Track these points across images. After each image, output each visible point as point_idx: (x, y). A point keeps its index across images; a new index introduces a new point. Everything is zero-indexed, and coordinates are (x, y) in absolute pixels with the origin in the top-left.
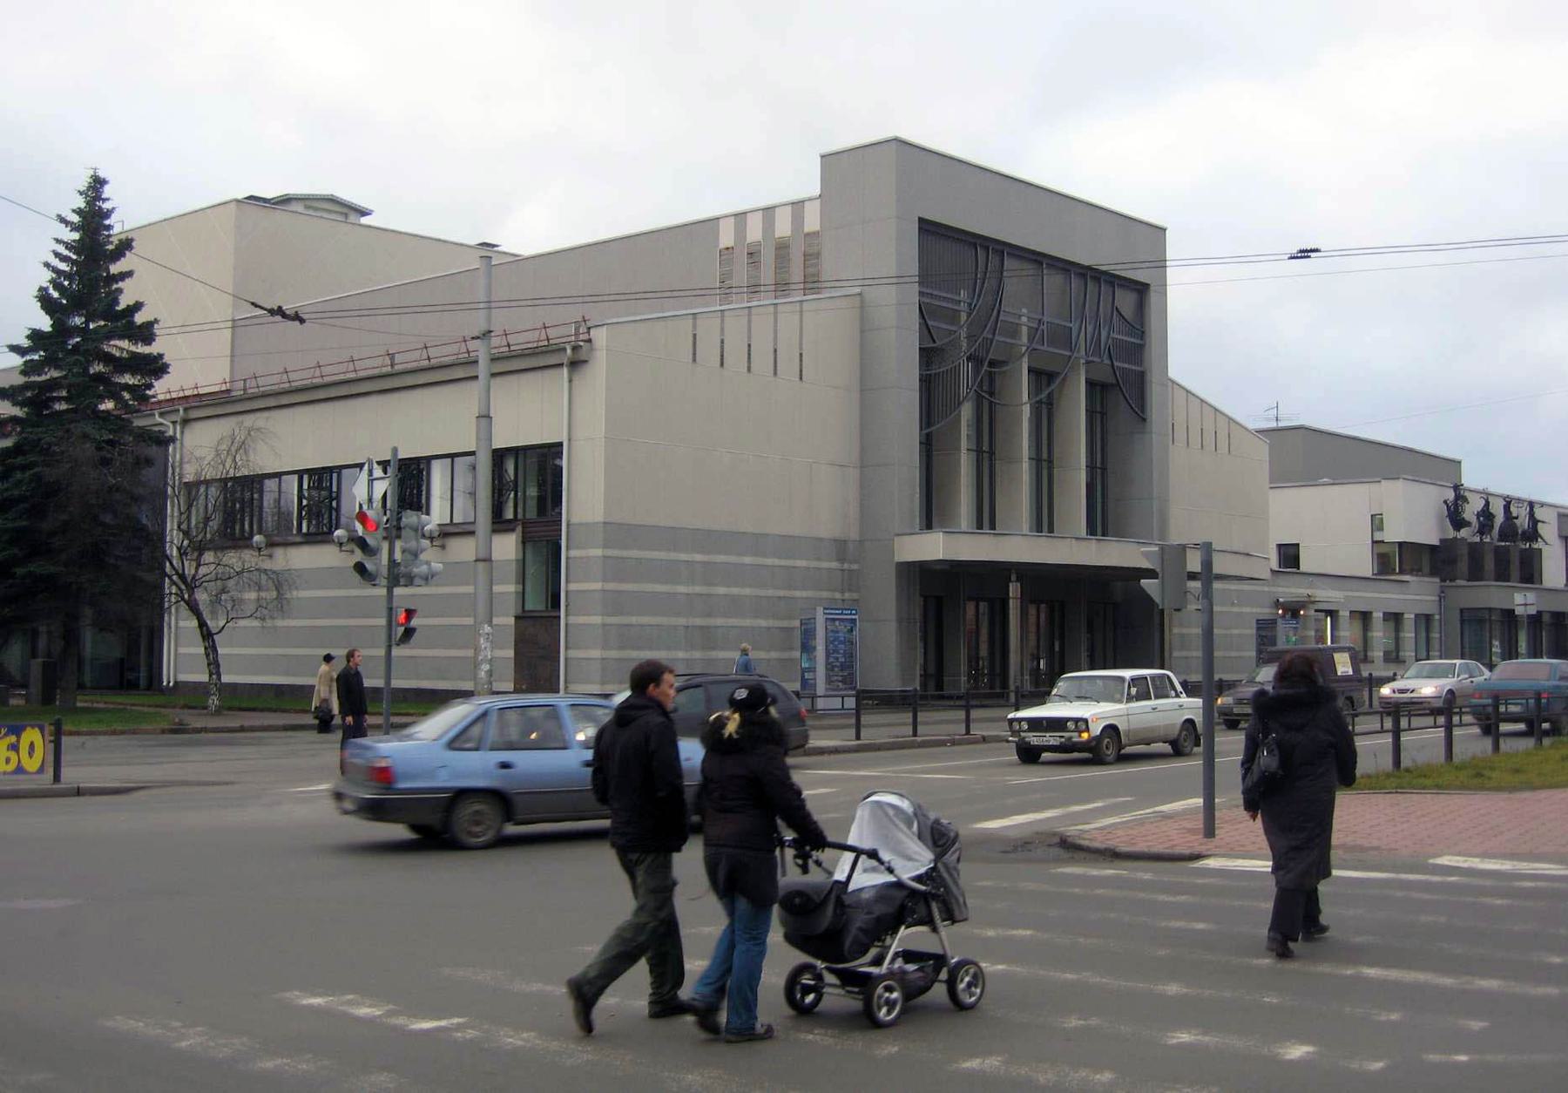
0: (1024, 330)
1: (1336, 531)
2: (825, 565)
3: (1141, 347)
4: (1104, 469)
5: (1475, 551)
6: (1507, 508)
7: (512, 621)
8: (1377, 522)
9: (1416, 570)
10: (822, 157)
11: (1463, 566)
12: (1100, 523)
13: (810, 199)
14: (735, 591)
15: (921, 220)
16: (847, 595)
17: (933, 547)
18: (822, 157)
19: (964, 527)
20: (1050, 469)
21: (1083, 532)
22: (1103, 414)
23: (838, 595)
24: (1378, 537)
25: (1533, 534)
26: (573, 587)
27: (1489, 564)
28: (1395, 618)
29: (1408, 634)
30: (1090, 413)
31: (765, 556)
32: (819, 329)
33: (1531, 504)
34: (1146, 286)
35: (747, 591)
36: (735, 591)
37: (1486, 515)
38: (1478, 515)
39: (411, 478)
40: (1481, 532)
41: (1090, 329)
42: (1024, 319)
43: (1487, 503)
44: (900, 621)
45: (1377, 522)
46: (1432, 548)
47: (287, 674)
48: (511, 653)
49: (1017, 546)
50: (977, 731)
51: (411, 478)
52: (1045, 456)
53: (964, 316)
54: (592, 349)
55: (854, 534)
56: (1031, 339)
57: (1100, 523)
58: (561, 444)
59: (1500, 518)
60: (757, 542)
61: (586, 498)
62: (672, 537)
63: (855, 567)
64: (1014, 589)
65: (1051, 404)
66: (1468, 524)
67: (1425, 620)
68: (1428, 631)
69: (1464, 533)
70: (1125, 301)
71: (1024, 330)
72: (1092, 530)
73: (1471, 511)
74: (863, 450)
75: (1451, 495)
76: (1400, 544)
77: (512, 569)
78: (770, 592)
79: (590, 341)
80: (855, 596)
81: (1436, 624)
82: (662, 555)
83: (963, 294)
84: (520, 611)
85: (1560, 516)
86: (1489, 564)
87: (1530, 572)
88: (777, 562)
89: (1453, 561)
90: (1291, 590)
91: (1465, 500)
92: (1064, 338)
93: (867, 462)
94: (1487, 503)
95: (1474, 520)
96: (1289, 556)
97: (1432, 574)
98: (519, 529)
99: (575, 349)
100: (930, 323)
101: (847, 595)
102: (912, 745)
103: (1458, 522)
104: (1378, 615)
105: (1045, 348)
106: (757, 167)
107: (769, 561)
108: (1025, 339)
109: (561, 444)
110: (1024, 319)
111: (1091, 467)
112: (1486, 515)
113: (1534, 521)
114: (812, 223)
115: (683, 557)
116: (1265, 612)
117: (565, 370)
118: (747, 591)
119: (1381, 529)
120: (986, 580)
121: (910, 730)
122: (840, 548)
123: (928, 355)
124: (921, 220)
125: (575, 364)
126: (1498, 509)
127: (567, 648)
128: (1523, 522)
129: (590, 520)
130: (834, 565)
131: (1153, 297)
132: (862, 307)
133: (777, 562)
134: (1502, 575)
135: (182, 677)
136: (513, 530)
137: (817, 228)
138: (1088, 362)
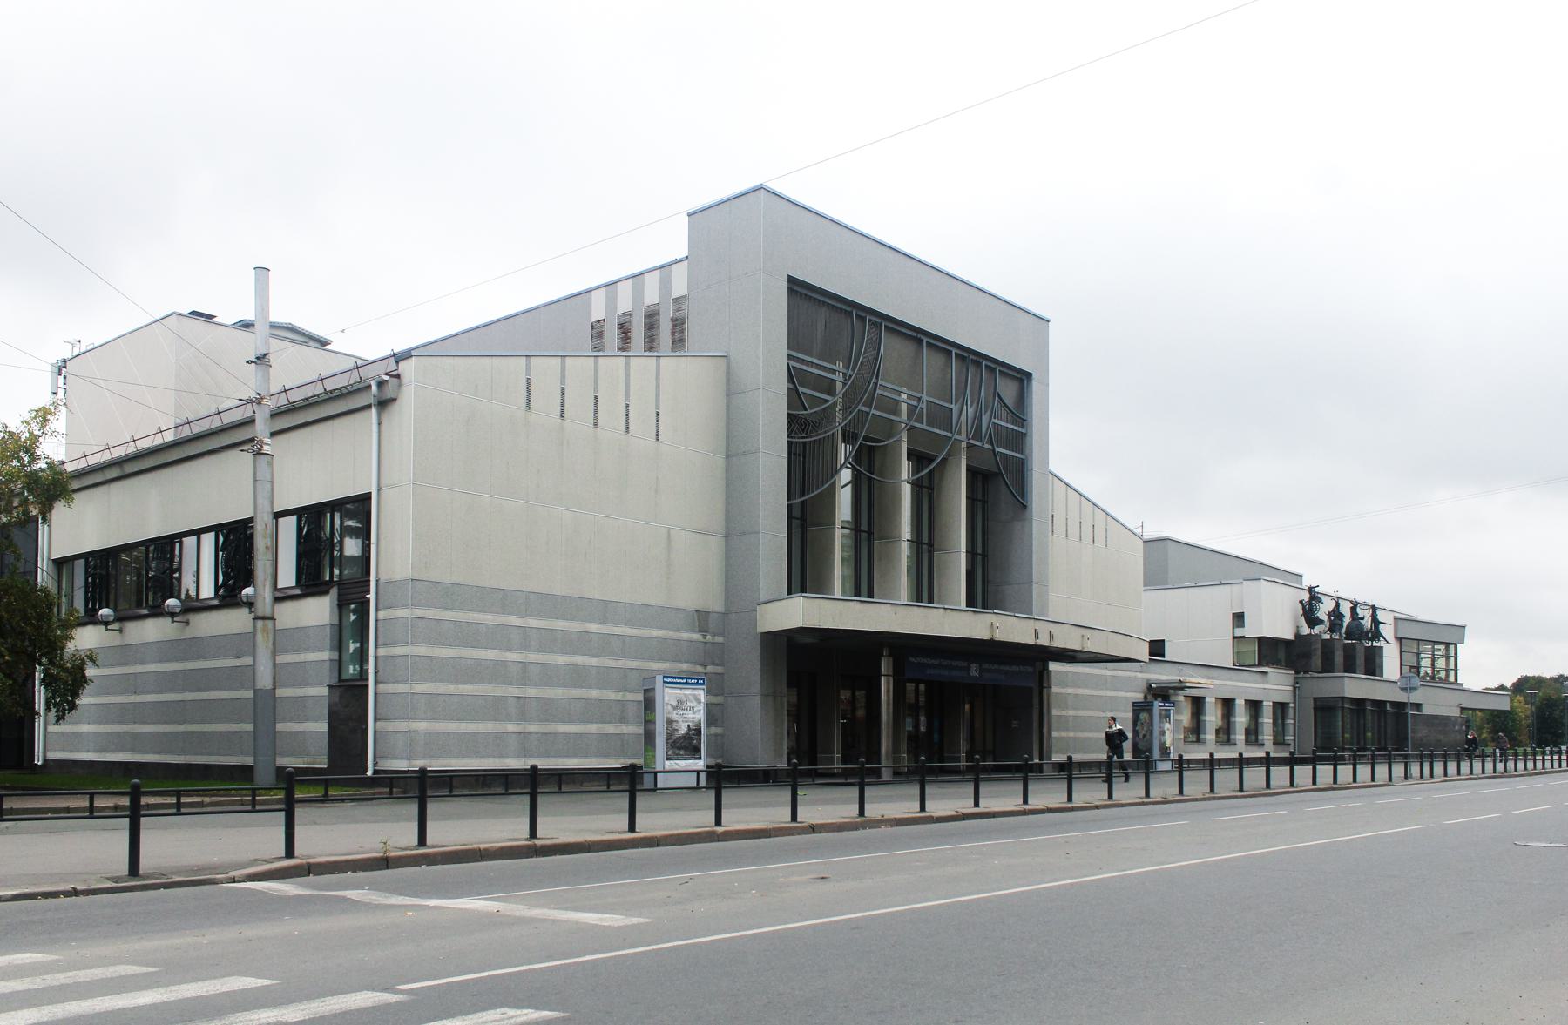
0: (904, 407)
1: (1198, 631)
2: (685, 636)
3: (1023, 435)
4: (984, 555)
5: (1327, 646)
6: (1353, 610)
7: (325, 691)
8: (1239, 619)
9: (1274, 663)
10: (689, 215)
11: (1317, 660)
12: (982, 595)
13: (677, 262)
14: (579, 660)
15: (792, 280)
16: (710, 669)
17: (798, 613)
18: (689, 215)
19: (838, 595)
20: (931, 553)
21: (963, 606)
22: (984, 502)
23: (700, 669)
24: (1239, 632)
25: (1377, 635)
26: (382, 652)
27: (1339, 658)
28: (1254, 706)
29: (1267, 720)
30: (971, 499)
31: (616, 624)
32: (679, 386)
33: (1374, 608)
34: (1029, 375)
35: (593, 661)
36: (579, 660)
37: (1336, 614)
38: (1329, 615)
39: (237, 541)
40: (1331, 630)
41: (971, 411)
42: (904, 396)
43: (1338, 605)
44: (764, 695)
45: (1239, 619)
46: (1286, 643)
47: (133, 751)
48: (324, 727)
49: (892, 615)
50: (872, 811)
51: (237, 541)
52: (925, 540)
53: (839, 386)
54: (400, 385)
55: (716, 605)
56: (909, 416)
57: (982, 595)
58: (367, 497)
59: (1347, 620)
60: (606, 610)
61: (396, 552)
62: (503, 600)
63: (719, 639)
64: (886, 666)
65: (931, 488)
66: (1322, 622)
67: (1280, 708)
68: (1284, 718)
69: (1317, 630)
70: (1007, 390)
71: (904, 407)
72: (971, 602)
73: (1323, 610)
74: (729, 518)
75: (1306, 597)
76: (1260, 639)
77: (327, 637)
78: (621, 663)
79: (398, 376)
80: (719, 669)
81: (1291, 712)
82: (489, 618)
83: (840, 366)
84: (335, 682)
85: (1396, 619)
86: (1339, 658)
87: (1372, 665)
88: (628, 631)
89: (1307, 656)
90: (1162, 675)
91: (1320, 600)
92: (943, 418)
93: (735, 534)
94: (1338, 605)
95: (1325, 618)
96: (1157, 648)
97: (1288, 666)
98: (334, 591)
99: (381, 384)
100: (801, 389)
101: (710, 669)
102: (709, 837)
103: (1312, 620)
104: (1240, 703)
105: (925, 427)
106: (633, 238)
107: (618, 630)
108: (904, 416)
109: (367, 497)
110: (904, 396)
111: (971, 553)
112: (1336, 614)
113: (1376, 622)
114: (679, 288)
115: (516, 621)
116: (1139, 697)
117: (374, 411)
118: (593, 661)
119: (1242, 625)
120: (859, 651)
121: (917, 806)
122: (701, 620)
123: (796, 424)
124: (792, 280)
125: (383, 404)
126: (1345, 609)
127: (376, 720)
128: (1367, 623)
129: (398, 577)
130: (696, 636)
131: (1035, 385)
132: (728, 367)
133: (628, 631)
134: (1350, 667)
135: (52, 756)
136: (326, 592)
137: (685, 292)
138: (970, 446)
